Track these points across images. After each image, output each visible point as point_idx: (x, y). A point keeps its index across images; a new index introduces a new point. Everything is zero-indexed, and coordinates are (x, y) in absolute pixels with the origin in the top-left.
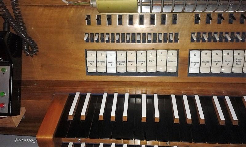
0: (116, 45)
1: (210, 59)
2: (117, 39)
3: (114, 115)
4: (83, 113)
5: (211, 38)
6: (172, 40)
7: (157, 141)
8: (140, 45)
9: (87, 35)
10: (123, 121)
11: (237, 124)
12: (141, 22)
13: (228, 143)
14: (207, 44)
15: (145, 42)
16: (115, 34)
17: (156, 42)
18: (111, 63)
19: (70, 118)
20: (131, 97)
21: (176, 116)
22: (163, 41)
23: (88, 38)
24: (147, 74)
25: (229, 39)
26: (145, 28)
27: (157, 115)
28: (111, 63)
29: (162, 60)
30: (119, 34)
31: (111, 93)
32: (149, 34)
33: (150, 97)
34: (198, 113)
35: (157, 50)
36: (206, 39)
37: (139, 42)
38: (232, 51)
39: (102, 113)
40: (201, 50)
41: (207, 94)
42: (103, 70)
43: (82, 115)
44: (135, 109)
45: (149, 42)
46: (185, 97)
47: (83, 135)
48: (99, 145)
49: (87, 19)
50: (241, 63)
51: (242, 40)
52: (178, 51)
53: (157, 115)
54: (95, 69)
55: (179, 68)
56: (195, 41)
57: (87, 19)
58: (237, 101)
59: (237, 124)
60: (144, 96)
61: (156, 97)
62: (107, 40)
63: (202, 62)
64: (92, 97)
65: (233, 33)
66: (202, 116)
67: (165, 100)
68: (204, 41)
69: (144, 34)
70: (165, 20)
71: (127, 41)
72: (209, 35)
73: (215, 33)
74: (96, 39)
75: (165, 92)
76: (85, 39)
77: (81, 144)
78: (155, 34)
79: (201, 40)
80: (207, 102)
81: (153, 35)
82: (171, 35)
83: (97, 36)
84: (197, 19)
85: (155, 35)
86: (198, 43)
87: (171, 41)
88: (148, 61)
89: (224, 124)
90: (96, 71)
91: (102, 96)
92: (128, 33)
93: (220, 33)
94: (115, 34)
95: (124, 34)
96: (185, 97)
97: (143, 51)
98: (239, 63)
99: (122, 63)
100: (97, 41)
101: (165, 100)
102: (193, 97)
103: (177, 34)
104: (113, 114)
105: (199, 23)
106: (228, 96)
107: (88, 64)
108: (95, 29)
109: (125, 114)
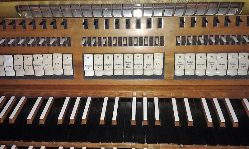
0: (101, 49)
1: (236, 62)
2: (124, 43)
4: (84, 117)
5: (207, 41)
6: (179, 44)
7: (134, 143)
8: (139, 48)
9: (84, 39)
10: (113, 124)
11: (192, 125)
12: (138, 26)
13: (41, 141)
14: (214, 47)
16: (112, 38)
17: (153, 45)
18: (8, 66)
20: (121, 100)
21: (177, 119)
23: (95, 42)
24: (143, 77)
25: (225, 41)
26: (143, 31)
27: (157, 118)
28: (8, 66)
29: (58, 64)
30: (116, 38)
31: (99, 96)
32: (145, 37)
33: (111, 101)
34: (218, 117)
35: (153, 54)
36: (202, 42)
37: (136, 45)
38: (227, 54)
39: (102, 117)
41: (196, 97)
42: (101, 74)
43: (71, 119)
44: (124, 112)
45: (146, 45)
46: (216, 101)
47: (39, 139)
48: (58, 148)
50: (130, 66)
51: (238, 42)
52: (164, 53)
53: (157, 118)
54: (92, 73)
57: (84, 24)
58: (238, 105)
59: (192, 125)
61: (156, 100)
62: (104, 44)
63: (189, 64)
64: (93, 100)
65: (218, 36)
66: (190, 119)
67: (165, 102)
68: (186, 43)
69: (141, 38)
70: (162, 23)
71: (134, 44)
72: (193, 38)
73: (233, 36)
74: (93, 43)
75: (166, 95)
76: (83, 43)
77: (29, 147)
78: (151, 38)
79: (197, 43)
80: (196, 104)
81: (150, 39)
82: (189, 38)
83: (94, 40)
84: (182, 21)
86: (183, 46)
88: (44, 65)
90: (62, 74)
91: (36, 99)
93: (216, 36)
94: (112, 38)
95: (121, 37)
96: (216, 101)
97: (140, 54)
98: (129, 66)
99: (19, 67)
100: (105, 45)
101: (165, 102)
103: (162, 38)
104: (145, 118)
105: (184, 27)
106: (228, 99)
107: (86, 68)
108: (92, 31)
109: (114, 118)
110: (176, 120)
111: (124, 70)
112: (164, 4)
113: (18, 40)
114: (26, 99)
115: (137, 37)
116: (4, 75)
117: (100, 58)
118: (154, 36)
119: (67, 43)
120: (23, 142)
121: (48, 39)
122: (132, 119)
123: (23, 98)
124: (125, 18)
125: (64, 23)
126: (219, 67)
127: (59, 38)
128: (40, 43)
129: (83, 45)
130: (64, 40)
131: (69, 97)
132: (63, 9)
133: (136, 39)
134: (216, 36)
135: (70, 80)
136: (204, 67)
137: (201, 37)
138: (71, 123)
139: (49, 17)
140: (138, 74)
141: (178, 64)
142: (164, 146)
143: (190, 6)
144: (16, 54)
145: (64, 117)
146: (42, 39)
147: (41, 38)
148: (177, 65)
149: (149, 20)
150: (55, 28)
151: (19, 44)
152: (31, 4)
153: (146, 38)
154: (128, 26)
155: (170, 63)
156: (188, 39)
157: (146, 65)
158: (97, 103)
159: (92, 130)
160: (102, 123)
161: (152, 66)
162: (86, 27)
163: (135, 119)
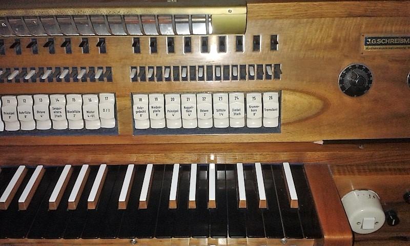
3: (175, 199)
7: (155, 238)
8: (213, 83)
10: (170, 208)
15: (212, 80)
17: (262, 79)
19: (294, 205)
22: (255, 77)
23: (136, 75)
26: (214, 57)
27: (262, 196)
28: (220, 110)
30: (169, 67)
33: (140, 170)
39: (173, 196)
40: (228, 93)
42: (161, 125)
43: (69, 201)
44: (227, 191)
49: (134, 45)
55: (132, 120)
56: (273, 77)
60: (212, 167)
67: (273, 171)
70: (242, 44)
78: (243, 67)
81: (224, 69)
85: (260, 66)
87: (268, 77)
89: (74, 207)
90: (50, 127)
91: (62, 168)
92: (234, 64)
98: (59, 114)
100: (151, 79)
101: (273, 171)
102: (206, 167)
103: (277, 66)
104: (192, 197)
107: (136, 116)
108: (147, 57)
110: (292, 199)
111: (230, 119)
112: (173, 16)
113: (25, 72)
114: (44, 170)
115: (203, 67)
116: (19, 129)
117: (143, 100)
118: (230, 63)
119: (105, 77)
120: (44, 239)
121: (75, 71)
122: (170, 199)
123: (39, 169)
124: (183, 36)
125: (102, 43)
126: (200, 115)
127: (75, 69)
128: (62, 77)
129: (149, 78)
130: (84, 71)
131: (70, 166)
132: (95, 21)
133: (201, 70)
134: (275, 65)
135: (275, 134)
136: (226, 114)
137: (270, 67)
138: (70, 208)
139: (41, 34)
140: (238, 124)
141: (138, 110)
142: (101, 242)
143: (133, 19)
144: (68, 94)
145: (129, 195)
146: (65, 70)
147: (13, 69)
148: (137, 112)
149: (170, 39)
150: (52, 52)
151: (26, 78)
152: (10, 15)
153: (184, 69)
154: (171, 49)
155: (125, 109)
156: (266, 70)
157: (87, 112)
158: (116, 173)
159: (106, 218)
160: (173, 206)
161: (96, 114)
162: (138, 51)
163: (214, 199)
